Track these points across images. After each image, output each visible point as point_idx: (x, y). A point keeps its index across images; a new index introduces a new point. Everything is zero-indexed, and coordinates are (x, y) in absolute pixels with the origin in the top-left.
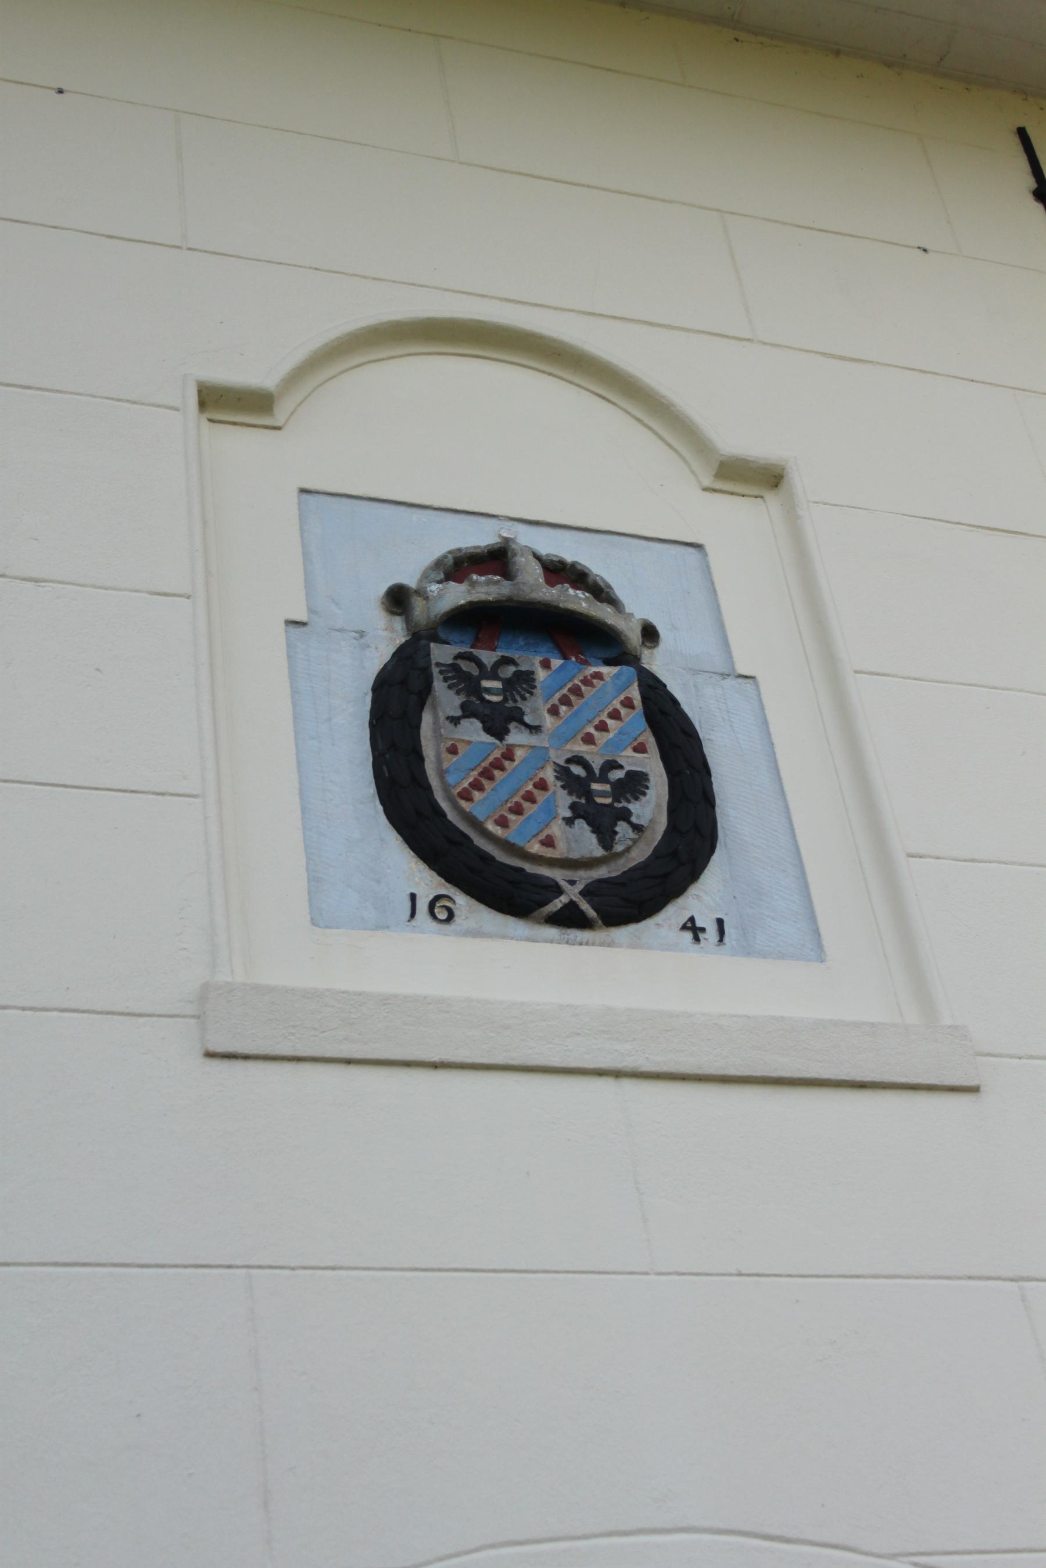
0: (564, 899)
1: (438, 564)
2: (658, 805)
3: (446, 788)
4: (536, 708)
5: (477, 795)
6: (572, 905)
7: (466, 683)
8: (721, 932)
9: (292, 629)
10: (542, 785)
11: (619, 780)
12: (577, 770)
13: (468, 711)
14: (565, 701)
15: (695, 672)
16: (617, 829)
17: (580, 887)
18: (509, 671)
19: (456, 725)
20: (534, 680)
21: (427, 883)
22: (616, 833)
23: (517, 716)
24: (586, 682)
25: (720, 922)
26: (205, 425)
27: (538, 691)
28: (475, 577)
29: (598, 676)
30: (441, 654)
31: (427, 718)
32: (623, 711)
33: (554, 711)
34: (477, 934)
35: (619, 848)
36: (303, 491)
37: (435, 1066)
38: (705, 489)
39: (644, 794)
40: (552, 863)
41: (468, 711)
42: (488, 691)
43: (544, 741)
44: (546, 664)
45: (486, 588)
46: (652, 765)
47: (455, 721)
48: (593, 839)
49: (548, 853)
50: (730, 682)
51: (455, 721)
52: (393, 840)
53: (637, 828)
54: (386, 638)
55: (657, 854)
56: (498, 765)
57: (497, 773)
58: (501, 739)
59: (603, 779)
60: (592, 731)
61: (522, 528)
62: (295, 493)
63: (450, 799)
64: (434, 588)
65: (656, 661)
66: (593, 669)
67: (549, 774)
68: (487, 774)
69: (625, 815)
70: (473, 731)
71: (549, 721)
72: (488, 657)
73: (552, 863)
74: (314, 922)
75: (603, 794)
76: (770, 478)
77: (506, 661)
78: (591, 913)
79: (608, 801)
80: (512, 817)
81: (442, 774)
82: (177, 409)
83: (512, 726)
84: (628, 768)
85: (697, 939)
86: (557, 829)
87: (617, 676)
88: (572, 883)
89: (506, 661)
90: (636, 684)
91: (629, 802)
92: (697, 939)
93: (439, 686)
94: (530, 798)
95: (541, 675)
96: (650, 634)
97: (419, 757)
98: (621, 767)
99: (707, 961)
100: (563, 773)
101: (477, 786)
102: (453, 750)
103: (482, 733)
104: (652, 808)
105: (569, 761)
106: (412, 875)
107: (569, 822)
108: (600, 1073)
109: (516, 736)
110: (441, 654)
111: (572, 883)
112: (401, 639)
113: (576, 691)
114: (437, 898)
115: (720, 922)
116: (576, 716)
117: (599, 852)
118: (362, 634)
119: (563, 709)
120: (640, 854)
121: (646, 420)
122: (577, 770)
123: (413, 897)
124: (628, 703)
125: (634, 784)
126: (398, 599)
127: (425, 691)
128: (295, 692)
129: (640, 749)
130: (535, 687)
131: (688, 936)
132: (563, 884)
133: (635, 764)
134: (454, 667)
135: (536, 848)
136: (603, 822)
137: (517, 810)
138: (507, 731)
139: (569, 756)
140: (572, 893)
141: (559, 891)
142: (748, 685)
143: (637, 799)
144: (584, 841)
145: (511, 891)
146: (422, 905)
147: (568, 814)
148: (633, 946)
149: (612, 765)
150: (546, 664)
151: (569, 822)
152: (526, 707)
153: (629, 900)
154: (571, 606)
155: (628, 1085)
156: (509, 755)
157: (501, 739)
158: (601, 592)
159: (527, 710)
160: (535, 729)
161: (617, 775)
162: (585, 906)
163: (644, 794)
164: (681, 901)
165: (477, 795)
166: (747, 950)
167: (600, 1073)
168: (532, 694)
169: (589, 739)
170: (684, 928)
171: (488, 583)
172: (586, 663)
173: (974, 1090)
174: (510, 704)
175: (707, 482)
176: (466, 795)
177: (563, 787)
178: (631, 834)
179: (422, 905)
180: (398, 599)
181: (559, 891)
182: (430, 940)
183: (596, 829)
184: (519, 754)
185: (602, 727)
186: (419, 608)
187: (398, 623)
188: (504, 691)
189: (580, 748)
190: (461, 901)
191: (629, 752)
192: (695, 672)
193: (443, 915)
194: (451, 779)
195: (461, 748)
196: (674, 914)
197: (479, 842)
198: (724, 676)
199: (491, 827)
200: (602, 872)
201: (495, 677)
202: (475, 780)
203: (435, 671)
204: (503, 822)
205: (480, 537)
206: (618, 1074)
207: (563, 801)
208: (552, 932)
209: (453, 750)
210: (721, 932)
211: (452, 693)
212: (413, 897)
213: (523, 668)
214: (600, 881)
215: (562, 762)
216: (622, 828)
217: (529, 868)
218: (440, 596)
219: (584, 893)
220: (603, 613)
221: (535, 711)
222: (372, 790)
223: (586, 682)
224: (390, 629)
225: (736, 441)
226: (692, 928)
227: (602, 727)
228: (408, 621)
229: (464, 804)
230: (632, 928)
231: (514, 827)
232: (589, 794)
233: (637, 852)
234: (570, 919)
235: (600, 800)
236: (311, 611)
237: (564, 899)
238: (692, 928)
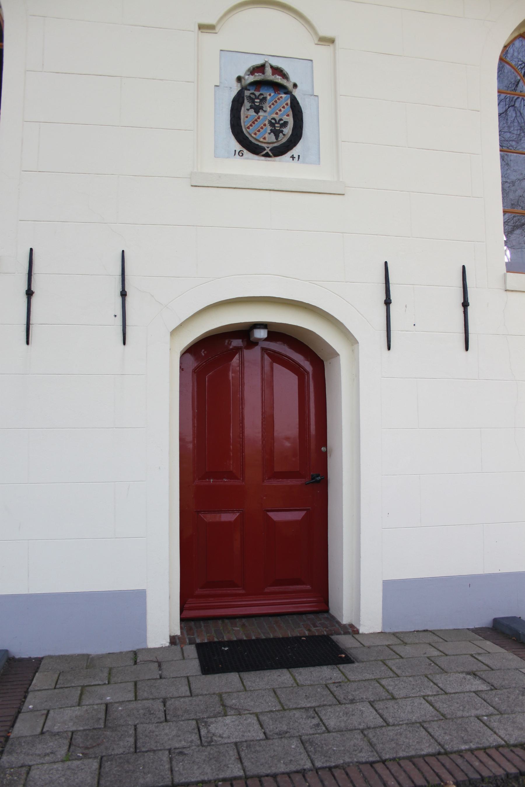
0: (266, 151)
1: (249, 70)
2: (290, 128)
3: (245, 126)
4: (266, 106)
5: (251, 128)
6: (267, 153)
8: (299, 158)
9: (216, 87)
10: (265, 125)
13: (251, 107)
14: (273, 104)
15: (305, 95)
17: (269, 148)
18: (261, 97)
21: (238, 147)
23: (262, 108)
24: (279, 99)
25: (299, 156)
26: (200, 33)
27: (267, 102)
28: (256, 74)
29: (281, 97)
30: (247, 93)
31: (243, 108)
32: (285, 106)
33: (270, 107)
34: (247, 159)
35: (279, 139)
36: (221, 50)
37: (234, 188)
38: (316, 44)
40: (265, 143)
41: (251, 107)
42: (256, 102)
43: (265, 116)
44: (270, 95)
45: (258, 77)
46: (290, 120)
47: (248, 110)
48: (274, 137)
49: (264, 141)
50: (313, 97)
51: (248, 110)
52: (233, 138)
53: (284, 135)
54: (236, 88)
55: (288, 141)
56: (256, 120)
57: (256, 122)
58: (257, 114)
59: (279, 123)
60: (278, 111)
61: (270, 57)
62: (219, 52)
63: (245, 128)
64: (247, 77)
65: (296, 93)
66: (281, 95)
67: (267, 122)
68: (254, 123)
69: (282, 132)
70: (252, 112)
71: (269, 109)
72: (257, 93)
73: (265, 143)
74: (215, 157)
75: (278, 127)
76: (331, 41)
77: (261, 94)
78: (271, 154)
79: (278, 128)
80: (257, 133)
81: (244, 122)
82: (193, 31)
83: (261, 111)
85: (293, 160)
86: (267, 135)
87: (285, 97)
88: (268, 148)
89: (261, 94)
92: (293, 160)
93: (246, 101)
94: (262, 128)
95: (269, 98)
96: (295, 86)
97: (240, 119)
98: (283, 120)
99: (295, 164)
100: (270, 122)
101: (251, 125)
102: (247, 117)
104: (288, 131)
106: (237, 146)
107: (269, 133)
108: (267, 190)
109: (261, 113)
110: (247, 93)
111: (268, 148)
112: (239, 89)
113: (276, 102)
115: (299, 156)
116: (276, 108)
117: (275, 141)
118: (231, 88)
119: (272, 106)
120: (284, 140)
121: (304, 24)
122: (273, 121)
124: (287, 104)
125: (285, 124)
126: (239, 79)
127: (243, 102)
128: (215, 103)
129: (288, 115)
131: (292, 159)
132: (266, 148)
134: (250, 96)
135: (262, 140)
136: (276, 133)
137: (259, 131)
138: (259, 112)
140: (268, 150)
141: (265, 150)
142: (316, 98)
144: (272, 138)
145: (255, 149)
146: (237, 153)
147: (270, 132)
148: (280, 161)
149: (281, 120)
150: (270, 95)
151: (269, 133)
152: (264, 106)
153: (279, 151)
154: (277, 81)
155: (272, 192)
156: (259, 118)
157: (257, 114)
158: (285, 76)
159: (264, 107)
160: (265, 111)
161: (282, 122)
162: (270, 153)
164: (291, 151)
165: (251, 128)
166: (304, 162)
167: (267, 190)
169: (277, 114)
171: (259, 75)
172: (279, 94)
173: (344, 195)
174: (261, 105)
175: (316, 42)
176: (248, 128)
178: (282, 136)
179: (237, 153)
180: (239, 79)
181: (265, 150)
182: (238, 160)
183: (275, 135)
184: (261, 117)
185: (280, 110)
186: (243, 81)
187: (239, 85)
188: (260, 102)
189: (274, 116)
190: (245, 151)
191: (285, 117)
192: (305, 95)
193: (241, 155)
194: (246, 124)
195: (249, 117)
196: (289, 154)
197: (251, 139)
198: (311, 95)
199: (253, 135)
200: (275, 145)
201: (258, 98)
203: (245, 97)
204: (255, 134)
205: (258, 61)
206: (270, 190)
207: (269, 128)
208: (263, 158)
209: (247, 117)
210: (299, 158)
213: (265, 96)
214: (275, 147)
216: (281, 135)
217: (260, 144)
218: (248, 79)
219: (270, 150)
220: (284, 82)
221: (266, 107)
222: (230, 126)
223: (279, 99)
224: (237, 86)
225: (323, 33)
226: (293, 157)
227: (280, 110)
228: (241, 84)
229: (248, 130)
230: (280, 157)
232: (275, 127)
234: (267, 155)
235: (277, 128)
236: (220, 83)
237: (266, 151)
238: (293, 157)
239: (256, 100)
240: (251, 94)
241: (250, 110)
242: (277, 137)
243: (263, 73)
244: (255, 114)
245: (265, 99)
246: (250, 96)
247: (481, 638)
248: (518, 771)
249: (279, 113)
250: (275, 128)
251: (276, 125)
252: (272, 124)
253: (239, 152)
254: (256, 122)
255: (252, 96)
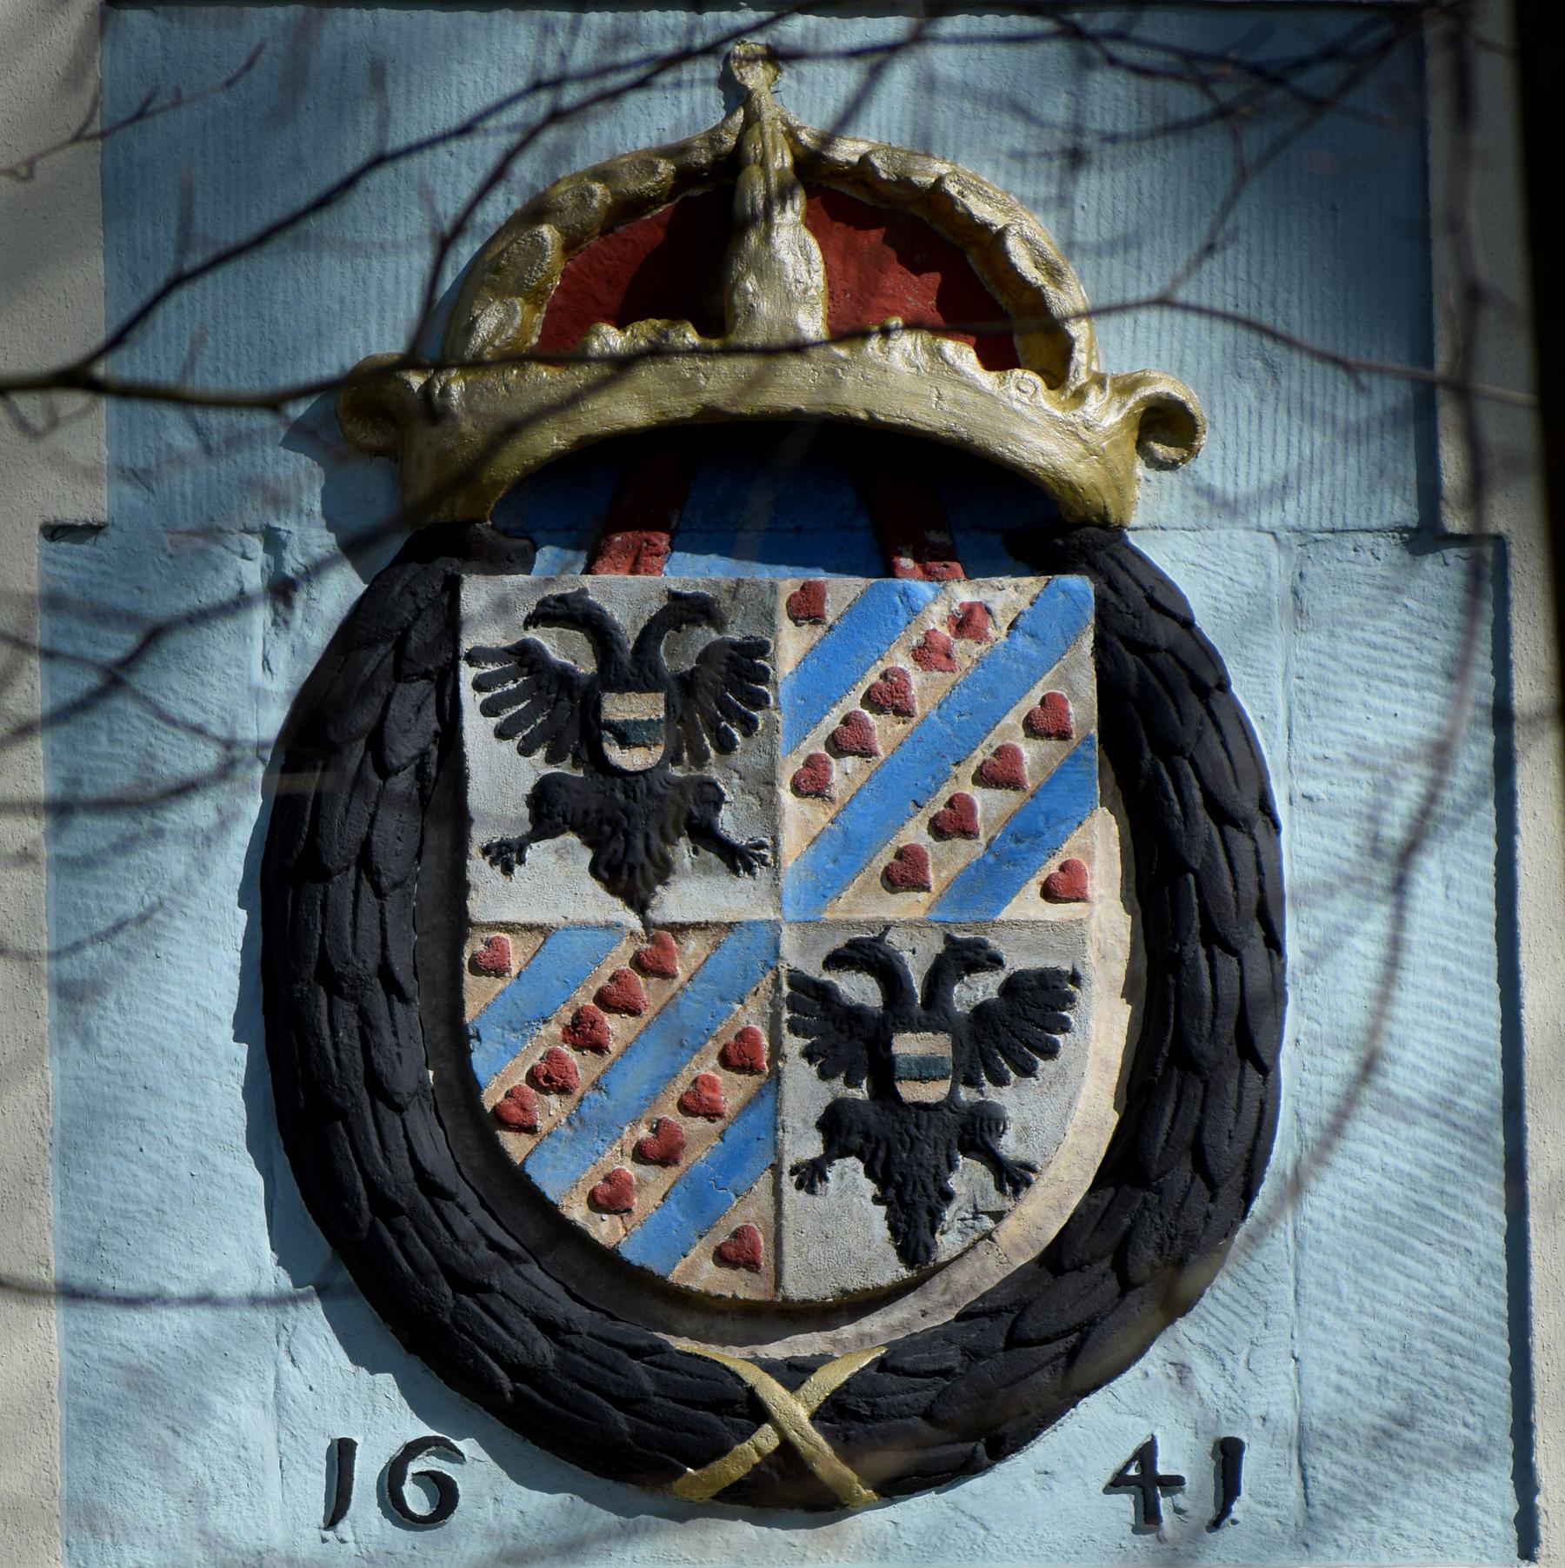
0: (766, 1439)
7: (560, 712)
11: (981, 1012)
12: (859, 989)
16: (954, 1182)
18: (682, 653)
19: (507, 870)
20: (763, 676)
22: (948, 1196)
32: (1030, 752)
35: (948, 1243)
39: (1050, 1052)
44: (807, 609)
57: (616, 1026)
69: (977, 1133)
75: (925, 1070)
77: (687, 610)
79: (933, 1092)
84: (1017, 961)
88: (794, 1373)
90: (1088, 642)
91: (1000, 1080)
95: (791, 646)
98: (996, 962)
103: (593, 887)
104: (1067, 1114)
105: (836, 961)
109: (692, 893)
111: (794, 1373)
114: (413, 1449)
117: (891, 1271)
122: (859, 989)
123: (343, 1452)
125: (1029, 1018)
130: (760, 701)
132: (772, 1392)
133: (1043, 948)
134: (525, 656)
136: (907, 1156)
138: (664, 871)
139: (839, 941)
141: (758, 1412)
143: (1027, 1071)
144: (840, 1230)
163: (1050, 1052)
168: (749, 726)
170: (1118, 1483)
177: (808, 1054)
185: (954, 823)
189: (865, 906)
193: (417, 1500)
202: (551, 1056)
211: (509, 747)
212: (343, 1452)
215: (813, 969)
227: (954, 823)
231: (645, 1202)
232: (883, 1073)
233: (1003, 1234)
235: (910, 1091)
237: (766, 1439)
239: (620, 708)
240: (550, 613)
241: (537, 852)
242: (912, 1213)
243: (715, 316)
244: (601, 906)
245: (744, 668)
246: (525, 656)
247: (448, 280)
248: (943, 1258)
249: (947, 862)
250: (884, 1089)
251: (907, 1045)
252: (850, 1041)
253: (394, 1475)
254: (616, 1026)
255: (557, 645)
